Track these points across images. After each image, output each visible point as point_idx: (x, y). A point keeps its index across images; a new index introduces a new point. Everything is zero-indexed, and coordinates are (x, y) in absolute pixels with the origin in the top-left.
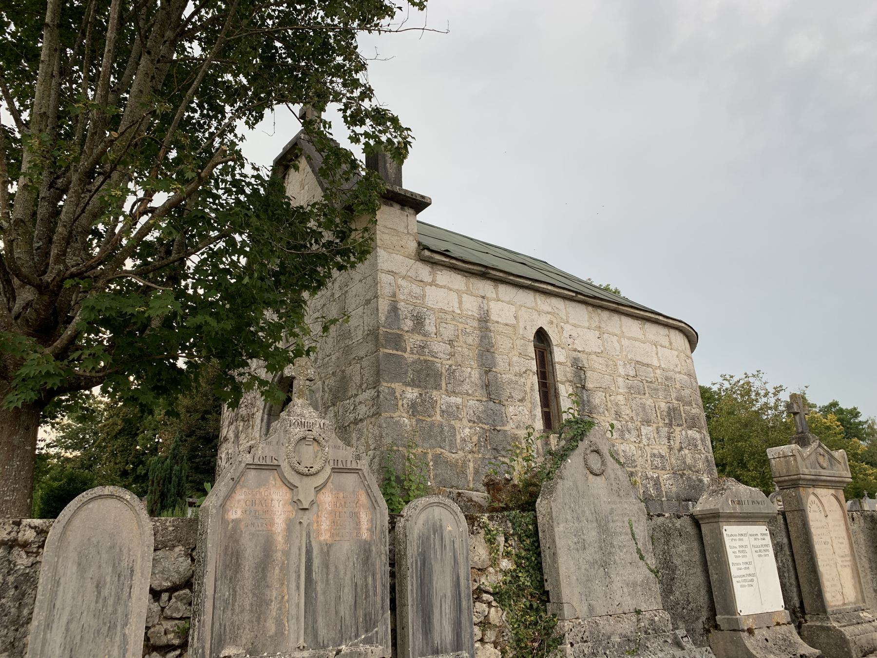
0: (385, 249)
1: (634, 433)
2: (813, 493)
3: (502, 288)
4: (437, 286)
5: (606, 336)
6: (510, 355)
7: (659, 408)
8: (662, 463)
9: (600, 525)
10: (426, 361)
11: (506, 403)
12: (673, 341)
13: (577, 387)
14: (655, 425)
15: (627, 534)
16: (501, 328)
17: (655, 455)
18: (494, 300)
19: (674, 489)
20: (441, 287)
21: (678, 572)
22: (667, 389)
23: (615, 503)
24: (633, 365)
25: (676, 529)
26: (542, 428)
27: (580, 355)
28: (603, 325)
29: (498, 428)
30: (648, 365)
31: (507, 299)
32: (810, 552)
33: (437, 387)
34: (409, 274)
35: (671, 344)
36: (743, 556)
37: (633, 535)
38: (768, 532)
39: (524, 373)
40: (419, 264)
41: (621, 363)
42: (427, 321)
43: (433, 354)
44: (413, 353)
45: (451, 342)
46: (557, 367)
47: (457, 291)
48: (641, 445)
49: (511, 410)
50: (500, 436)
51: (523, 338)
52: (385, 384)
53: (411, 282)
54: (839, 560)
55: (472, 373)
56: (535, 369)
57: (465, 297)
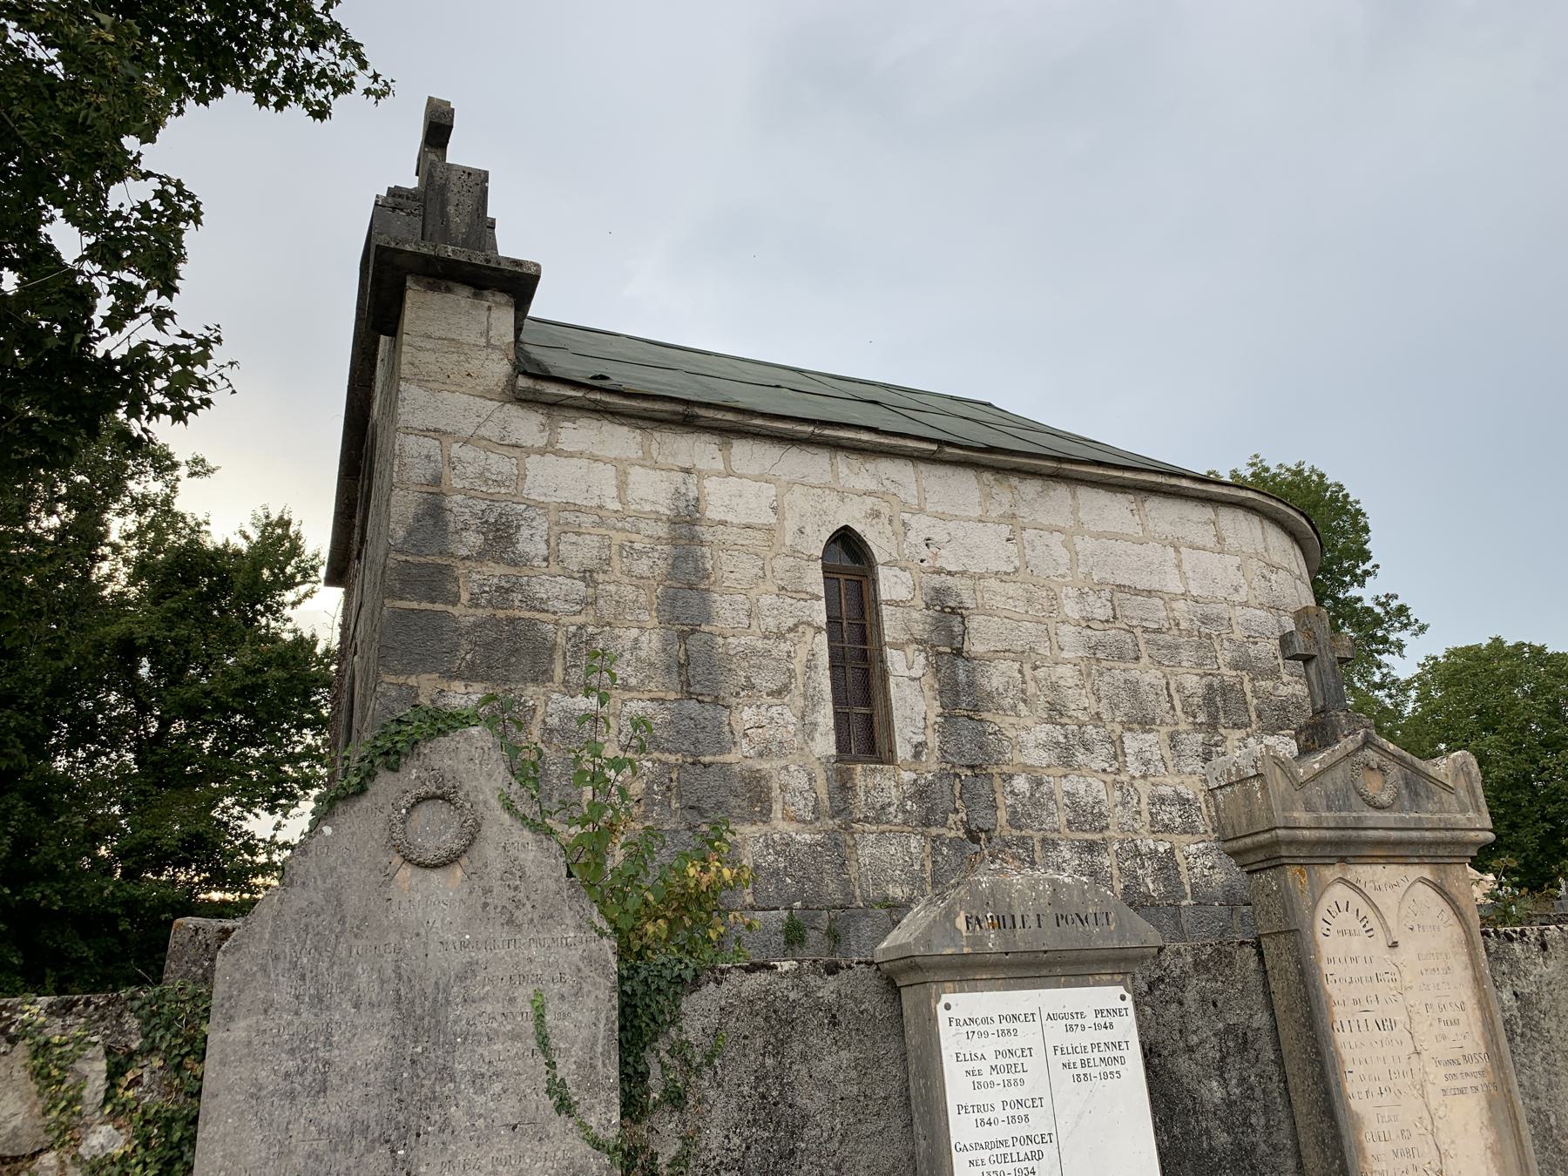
0: (421, 382)
1: (1102, 751)
2: (1343, 881)
3: (742, 451)
4: (559, 453)
5: (1030, 534)
6: (752, 594)
7: (1180, 689)
8: (1186, 815)
9: (406, 1018)
10: (511, 621)
11: (733, 701)
12: (1228, 533)
13: (940, 653)
14: (1164, 730)
15: (515, 1036)
16: (731, 535)
17: (1162, 800)
18: (719, 474)
19: (1219, 877)
20: (571, 455)
21: (810, 1133)
22: (1204, 644)
23: (490, 944)
24: (1106, 594)
25: (818, 1006)
26: (834, 751)
27: (950, 581)
28: (1023, 511)
29: (707, 759)
30: (1149, 593)
31: (755, 469)
32: (1318, 1053)
33: (541, 676)
34: (483, 432)
35: (1220, 539)
36: (1007, 1084)
37: (543, 1042)
38: (1129, 1003)
39: (790, 630)
40: (513, 410)
41: (1073, 592)
42: (525, 532)
43: (532, 603)
44: (477, 606)
45: (587, 576)
46: (886, 611)
47: (615, 462)
48: (1124, 778)
49: (747, 716)
50: (711, 778)
51: (794, 553)
52: (392, 679)
53: (486, 450)
54: (1437, 1074)
55: (641, 639)
56: (821, 618)
57: (636, 474)
